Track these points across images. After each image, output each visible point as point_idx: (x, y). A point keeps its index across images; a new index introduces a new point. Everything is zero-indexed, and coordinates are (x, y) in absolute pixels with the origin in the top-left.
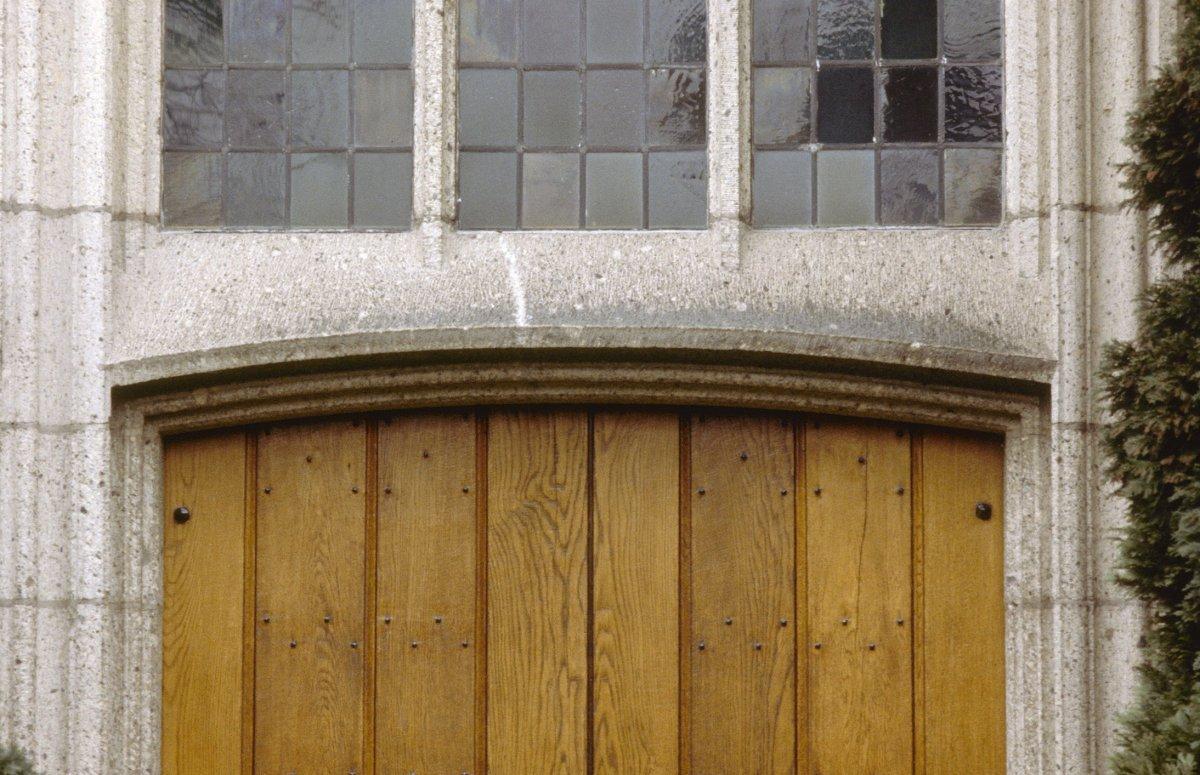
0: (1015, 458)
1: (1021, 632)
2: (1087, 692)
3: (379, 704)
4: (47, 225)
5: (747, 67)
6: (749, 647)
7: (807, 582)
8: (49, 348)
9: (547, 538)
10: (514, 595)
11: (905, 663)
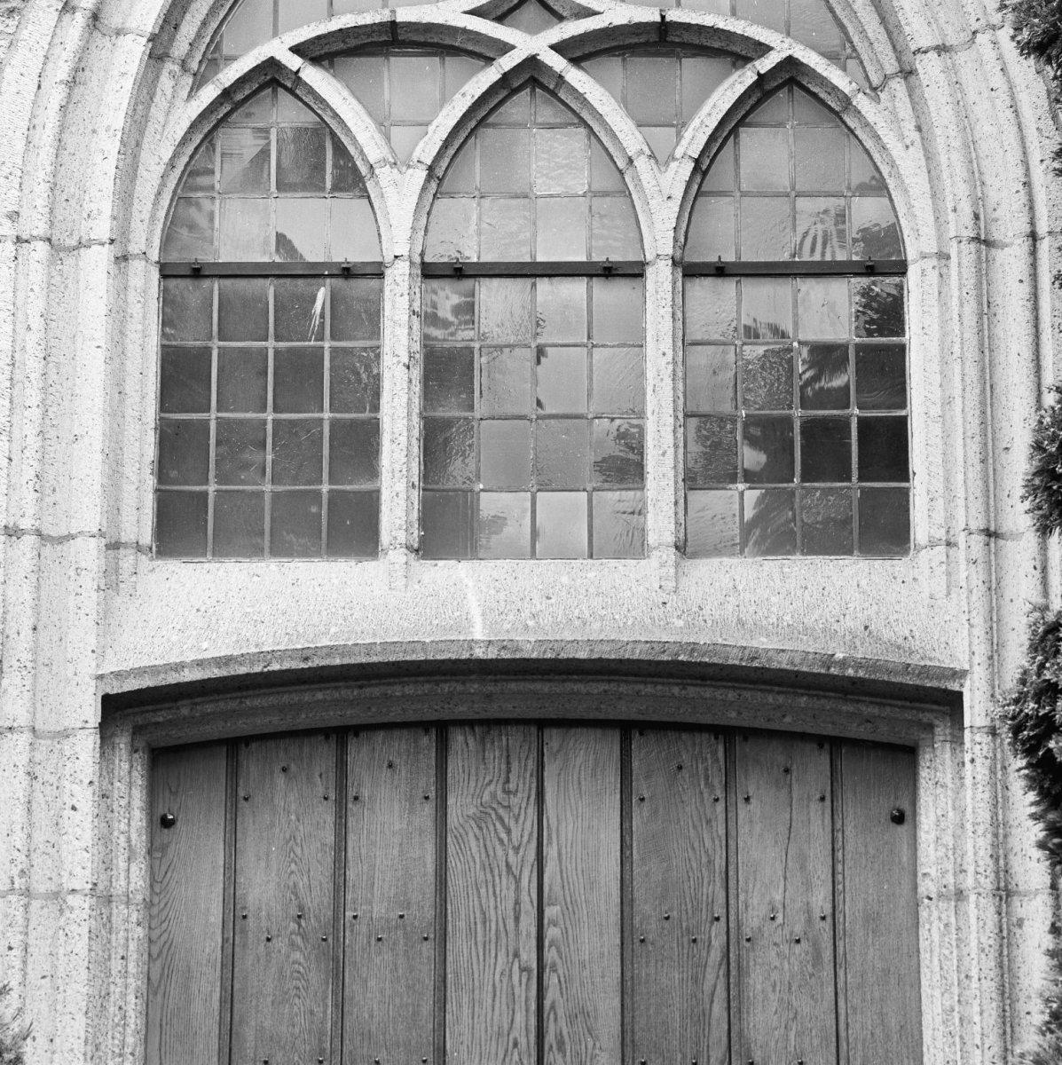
0: (928, 764)
1: (936, 923)
2: (1002, 976)
3: (346, 993)
4: (47, 551)
5: (681, 416)
6: (685, 939)
7: (738, 881)
8: (47, 662)
9: (501, 840)
10: (470, 892)
11: (827, 955)
